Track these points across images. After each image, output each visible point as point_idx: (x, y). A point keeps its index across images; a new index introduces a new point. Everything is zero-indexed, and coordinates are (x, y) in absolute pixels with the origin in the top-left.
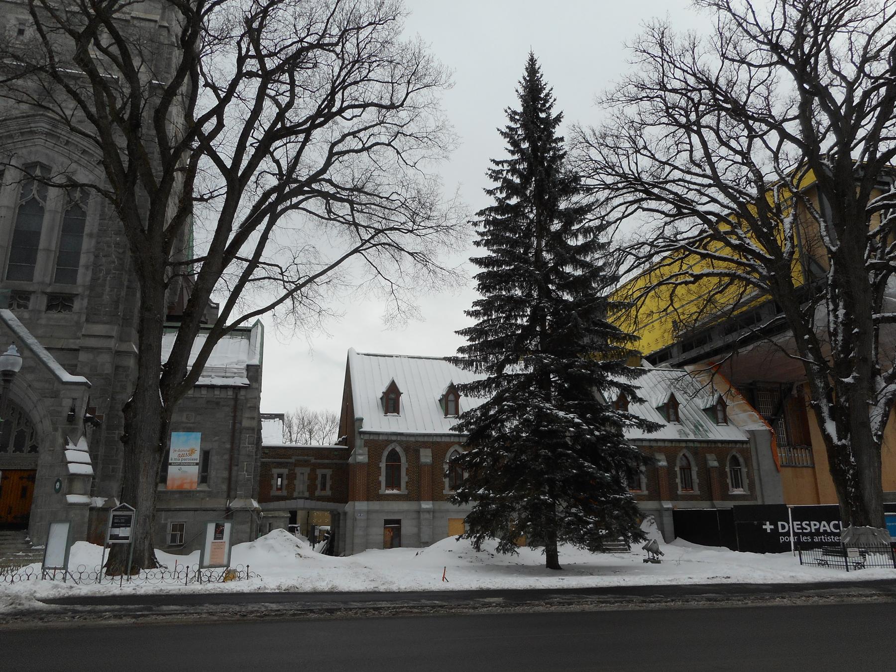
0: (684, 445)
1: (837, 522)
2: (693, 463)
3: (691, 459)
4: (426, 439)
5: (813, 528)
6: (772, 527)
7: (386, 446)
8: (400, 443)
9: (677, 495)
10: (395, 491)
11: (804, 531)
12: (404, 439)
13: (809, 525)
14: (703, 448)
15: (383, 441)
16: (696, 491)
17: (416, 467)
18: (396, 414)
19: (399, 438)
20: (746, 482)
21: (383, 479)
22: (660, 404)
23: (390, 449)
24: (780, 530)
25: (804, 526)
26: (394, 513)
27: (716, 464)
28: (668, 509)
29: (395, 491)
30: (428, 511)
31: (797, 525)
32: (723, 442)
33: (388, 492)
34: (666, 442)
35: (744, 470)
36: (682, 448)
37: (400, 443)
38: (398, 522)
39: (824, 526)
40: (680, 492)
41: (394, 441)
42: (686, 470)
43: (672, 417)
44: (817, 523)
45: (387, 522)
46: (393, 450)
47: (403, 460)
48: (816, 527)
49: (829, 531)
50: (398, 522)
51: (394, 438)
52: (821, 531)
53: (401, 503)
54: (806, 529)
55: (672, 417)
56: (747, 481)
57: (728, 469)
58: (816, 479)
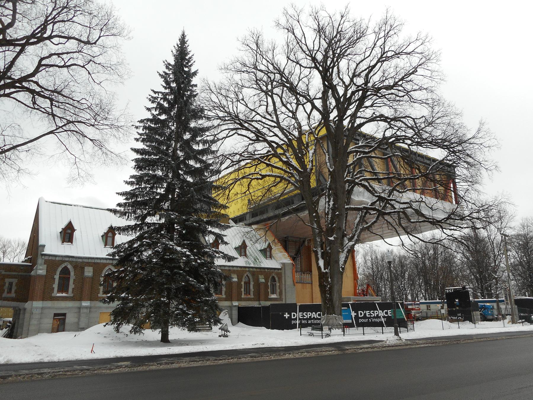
0: (247, 269)
3: (251, 277)
4: (90, 261)
6: (289, 315)
7: (61, 264)
8: (71, 263)
9: (241, 298)
10: (64, 295)
12: (74, 260)
14: (258, 271)
15: (59, 261)
16: (252, 296)
17: (81, 279)
19: (71, 259)
20: (278, 291)
21: (56, 286)
22: (237, 246)
23: (64, 266)
24: (360, 316)
26: (62, 308)
27: (263, 281)
28: (236, 306)
29: (64, 295)
30: (86, 307)
32: (268, 269)
33: (58, 295)
37: (71, 263)
38: (64, 315)
39: (314, 315)
40: (243, 296)
41: (67, 261)
42: (247, 283)
43: (243, 254)
45: (55, 315)
47: (72, 274)
48: (310, 315)
49: (316, 317)
50: (64, 315)
51: (67, 259)
54: (372, 315)
55: (243, 254)
57: (269, 284)
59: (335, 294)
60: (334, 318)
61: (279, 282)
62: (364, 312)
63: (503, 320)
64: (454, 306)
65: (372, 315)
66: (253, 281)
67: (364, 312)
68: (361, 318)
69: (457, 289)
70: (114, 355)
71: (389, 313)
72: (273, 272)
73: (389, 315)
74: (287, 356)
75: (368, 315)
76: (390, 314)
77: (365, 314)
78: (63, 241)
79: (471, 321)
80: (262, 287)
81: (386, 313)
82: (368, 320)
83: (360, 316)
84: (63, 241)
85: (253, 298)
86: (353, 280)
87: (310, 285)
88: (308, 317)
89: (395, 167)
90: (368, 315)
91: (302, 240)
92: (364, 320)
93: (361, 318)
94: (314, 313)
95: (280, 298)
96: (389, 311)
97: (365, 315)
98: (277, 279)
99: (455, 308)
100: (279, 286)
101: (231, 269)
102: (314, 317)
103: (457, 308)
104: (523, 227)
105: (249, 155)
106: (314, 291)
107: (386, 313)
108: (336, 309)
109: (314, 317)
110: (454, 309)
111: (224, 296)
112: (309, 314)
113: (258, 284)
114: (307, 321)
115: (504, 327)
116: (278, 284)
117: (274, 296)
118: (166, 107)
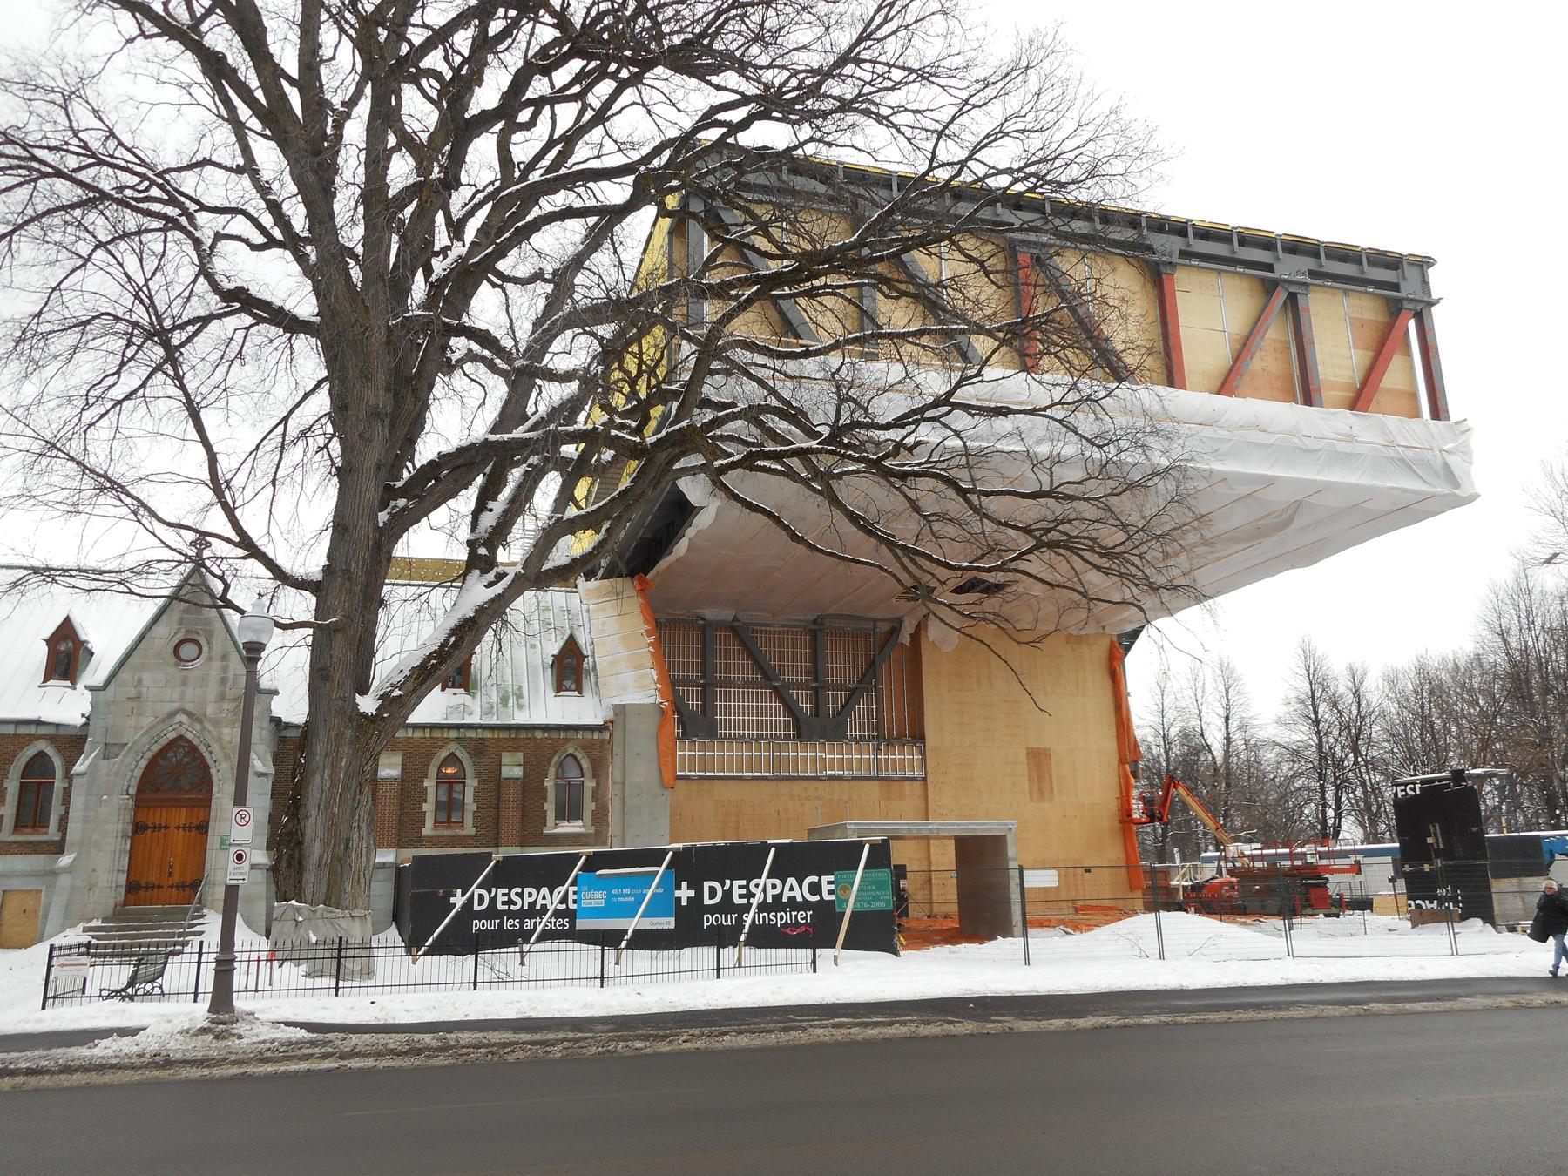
0: (453, 734)
1: (815, 879)
2: (469, 771)
5: (527, 900)
6: (692, 893)
8: (52, 739)
9: (420, 836)
11: (512, 908)
13: (520, 895)
14: (498, 740)
18: (68, 683)
20: (589, 806)
21: (549, 807)
24: (707, 901)
25: (514, 897)
28: (383, 866)
31: (740, 887)
32: (545, 728)
34: (428, 731)
35: (589, 784)
36: (446, 741)
37: (52, 739)
39: (792, 889)
40: (428, 830)
44: (533, 891)
46: (41, 755)
48: (777, 891)
49: (799, 899)
52: (785, 899)
53: (9, 858)
54: (515, 904)
56: (593, 806)
58: (926, 801)
59: (314, 813)
60: (290, 913)
62: (723, 885)
64: (1424, 855)
65: (515, 904)
66: (478, 775)
67: (723, 885)
68: (712, 910)
69: (1433, 780)
70: (964, 986)
71: (825, 888)
72: (567, 740)
73: (827, 897)
74: (730, 1041)
75: (741, 896)
76: (830, 892)
77: (728, 894)
78: (559, 688)
79: (1489, 918)
80: (511, 797)
81: (815, 888)
82: (500, 925)
83: (707, 901)
84: (559, 688)
85: (471, 837)
87: (918, 785)
88: (526, 907)
90: (741, 896)
91: (884, 628)
92: (721, 919)
93: (712, 910)
94: (792, 881)
95: (597, 833)
96: (825, 879)
97: (493, 900)
99: (1429, 860)
102: (792, 899)
103: (1439, 863)
105: (791, 366)
106: (931, 807)
107: (815, 888)
108: (309, 878)
109: (792, 899)
110: (1427, 868)
111: (472, 831)
112: (530, 895)
113: (493, 785)
114: (522, 923)
117: (567, 828)
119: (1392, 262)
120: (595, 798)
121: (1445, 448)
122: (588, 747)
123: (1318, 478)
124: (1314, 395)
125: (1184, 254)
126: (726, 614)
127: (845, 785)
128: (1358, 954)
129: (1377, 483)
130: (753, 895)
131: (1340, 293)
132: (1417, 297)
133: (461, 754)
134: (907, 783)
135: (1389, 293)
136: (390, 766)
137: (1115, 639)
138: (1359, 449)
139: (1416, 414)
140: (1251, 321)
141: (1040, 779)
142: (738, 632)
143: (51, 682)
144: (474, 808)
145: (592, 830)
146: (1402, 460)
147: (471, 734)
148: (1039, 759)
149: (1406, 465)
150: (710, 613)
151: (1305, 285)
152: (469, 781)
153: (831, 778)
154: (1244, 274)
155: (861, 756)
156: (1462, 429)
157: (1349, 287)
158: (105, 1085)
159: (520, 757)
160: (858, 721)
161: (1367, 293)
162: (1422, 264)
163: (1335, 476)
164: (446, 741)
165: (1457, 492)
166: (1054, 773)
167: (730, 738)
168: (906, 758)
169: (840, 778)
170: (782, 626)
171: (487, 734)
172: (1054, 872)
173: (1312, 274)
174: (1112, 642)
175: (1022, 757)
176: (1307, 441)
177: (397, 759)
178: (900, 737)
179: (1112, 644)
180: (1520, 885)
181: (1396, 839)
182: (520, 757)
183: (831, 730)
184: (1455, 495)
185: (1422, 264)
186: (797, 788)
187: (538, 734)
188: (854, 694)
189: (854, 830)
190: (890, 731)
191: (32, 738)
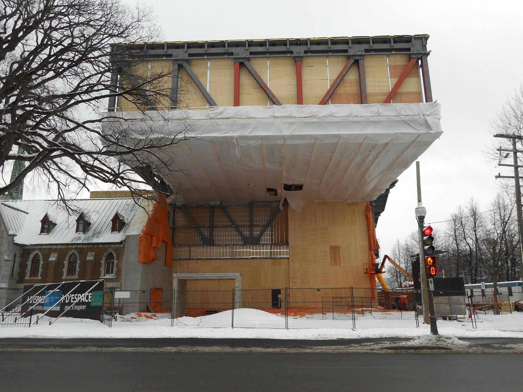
5: (79, 299)
8: (40, 249)
13: (77, 297)
20: (115, 269)
21: (65, 270)
36: (71, 249)
61: (118, 259)
63: (8, 289)
66: (80, 260)
72: (109, 248)
86: (367, 249)
89: (106, 38)
98: (115, 255)
100: (117, 265)
101: (53, 247)
104: (259, 102)
113: (84, 263)
115: (287, 328)
116: (116, 262)
118: (3, 47)
119: (407, 39)
120: (117, 267)
121: (426, 114)
122: (116, 250)
123: (365, 133)
124: (364, 99)
125: (306, 52)
126: (218, 203)
127: (258, 261)
128: (253, 327)
129: (390, 132)
130: (75, 300)
131: (326, 57)
132: (419, 52)
133: (76, 253)
134: (282, 260)
135: (407, 52)
136: (53, 257)
137: (369, 203)
138: (381, 119)
139: (421, 101)
140: (253, 77)
141: (335, 257)
142: (223, 207)
143: (42, 234)
144: (79, 270)
145: (115, 277)
146: (404, 121)
147: (79, 246)
148: (335, 250)
149: (406, 123)
150: (212, 203)
151: (363, 56)
152: (78, 261)
153: (253, 258)
154: (404, 54)
155: (265, 251)
156: (436, 104)
157: (388, 53)
158: (85, 353)
159: (93, 253)
160: (266, 238)
161: (371, 55)
162: (423, 39)
163: (370, 131)
164: (71, 249)
165: (430, 131)
166: (341, 255)
167: (266, 245)
168: (283, 251)
169: (256, 258)
170: (236, 206)
171: (84, 246)
172: (129, 292)
173: (366, 51)
174: (367, 204)
175: (328, 249)
176: (355, 118)
177: (56, 255)
178: (278, 243)
179: (367, 206)
180: (449, 299)
181: (412, 279)
182: (93, 253)
183: (254, 241)
184: (430, 133)
185: (423, 39)
186: (240, 262)
187: (100, 246)
188: (265, 227)
189: (176, 277)
190: (275, 242)
191: (34, 250)
